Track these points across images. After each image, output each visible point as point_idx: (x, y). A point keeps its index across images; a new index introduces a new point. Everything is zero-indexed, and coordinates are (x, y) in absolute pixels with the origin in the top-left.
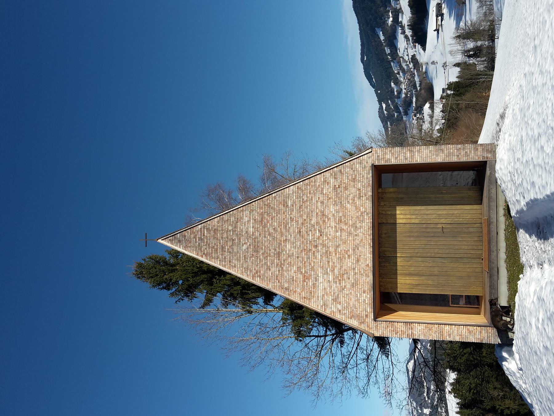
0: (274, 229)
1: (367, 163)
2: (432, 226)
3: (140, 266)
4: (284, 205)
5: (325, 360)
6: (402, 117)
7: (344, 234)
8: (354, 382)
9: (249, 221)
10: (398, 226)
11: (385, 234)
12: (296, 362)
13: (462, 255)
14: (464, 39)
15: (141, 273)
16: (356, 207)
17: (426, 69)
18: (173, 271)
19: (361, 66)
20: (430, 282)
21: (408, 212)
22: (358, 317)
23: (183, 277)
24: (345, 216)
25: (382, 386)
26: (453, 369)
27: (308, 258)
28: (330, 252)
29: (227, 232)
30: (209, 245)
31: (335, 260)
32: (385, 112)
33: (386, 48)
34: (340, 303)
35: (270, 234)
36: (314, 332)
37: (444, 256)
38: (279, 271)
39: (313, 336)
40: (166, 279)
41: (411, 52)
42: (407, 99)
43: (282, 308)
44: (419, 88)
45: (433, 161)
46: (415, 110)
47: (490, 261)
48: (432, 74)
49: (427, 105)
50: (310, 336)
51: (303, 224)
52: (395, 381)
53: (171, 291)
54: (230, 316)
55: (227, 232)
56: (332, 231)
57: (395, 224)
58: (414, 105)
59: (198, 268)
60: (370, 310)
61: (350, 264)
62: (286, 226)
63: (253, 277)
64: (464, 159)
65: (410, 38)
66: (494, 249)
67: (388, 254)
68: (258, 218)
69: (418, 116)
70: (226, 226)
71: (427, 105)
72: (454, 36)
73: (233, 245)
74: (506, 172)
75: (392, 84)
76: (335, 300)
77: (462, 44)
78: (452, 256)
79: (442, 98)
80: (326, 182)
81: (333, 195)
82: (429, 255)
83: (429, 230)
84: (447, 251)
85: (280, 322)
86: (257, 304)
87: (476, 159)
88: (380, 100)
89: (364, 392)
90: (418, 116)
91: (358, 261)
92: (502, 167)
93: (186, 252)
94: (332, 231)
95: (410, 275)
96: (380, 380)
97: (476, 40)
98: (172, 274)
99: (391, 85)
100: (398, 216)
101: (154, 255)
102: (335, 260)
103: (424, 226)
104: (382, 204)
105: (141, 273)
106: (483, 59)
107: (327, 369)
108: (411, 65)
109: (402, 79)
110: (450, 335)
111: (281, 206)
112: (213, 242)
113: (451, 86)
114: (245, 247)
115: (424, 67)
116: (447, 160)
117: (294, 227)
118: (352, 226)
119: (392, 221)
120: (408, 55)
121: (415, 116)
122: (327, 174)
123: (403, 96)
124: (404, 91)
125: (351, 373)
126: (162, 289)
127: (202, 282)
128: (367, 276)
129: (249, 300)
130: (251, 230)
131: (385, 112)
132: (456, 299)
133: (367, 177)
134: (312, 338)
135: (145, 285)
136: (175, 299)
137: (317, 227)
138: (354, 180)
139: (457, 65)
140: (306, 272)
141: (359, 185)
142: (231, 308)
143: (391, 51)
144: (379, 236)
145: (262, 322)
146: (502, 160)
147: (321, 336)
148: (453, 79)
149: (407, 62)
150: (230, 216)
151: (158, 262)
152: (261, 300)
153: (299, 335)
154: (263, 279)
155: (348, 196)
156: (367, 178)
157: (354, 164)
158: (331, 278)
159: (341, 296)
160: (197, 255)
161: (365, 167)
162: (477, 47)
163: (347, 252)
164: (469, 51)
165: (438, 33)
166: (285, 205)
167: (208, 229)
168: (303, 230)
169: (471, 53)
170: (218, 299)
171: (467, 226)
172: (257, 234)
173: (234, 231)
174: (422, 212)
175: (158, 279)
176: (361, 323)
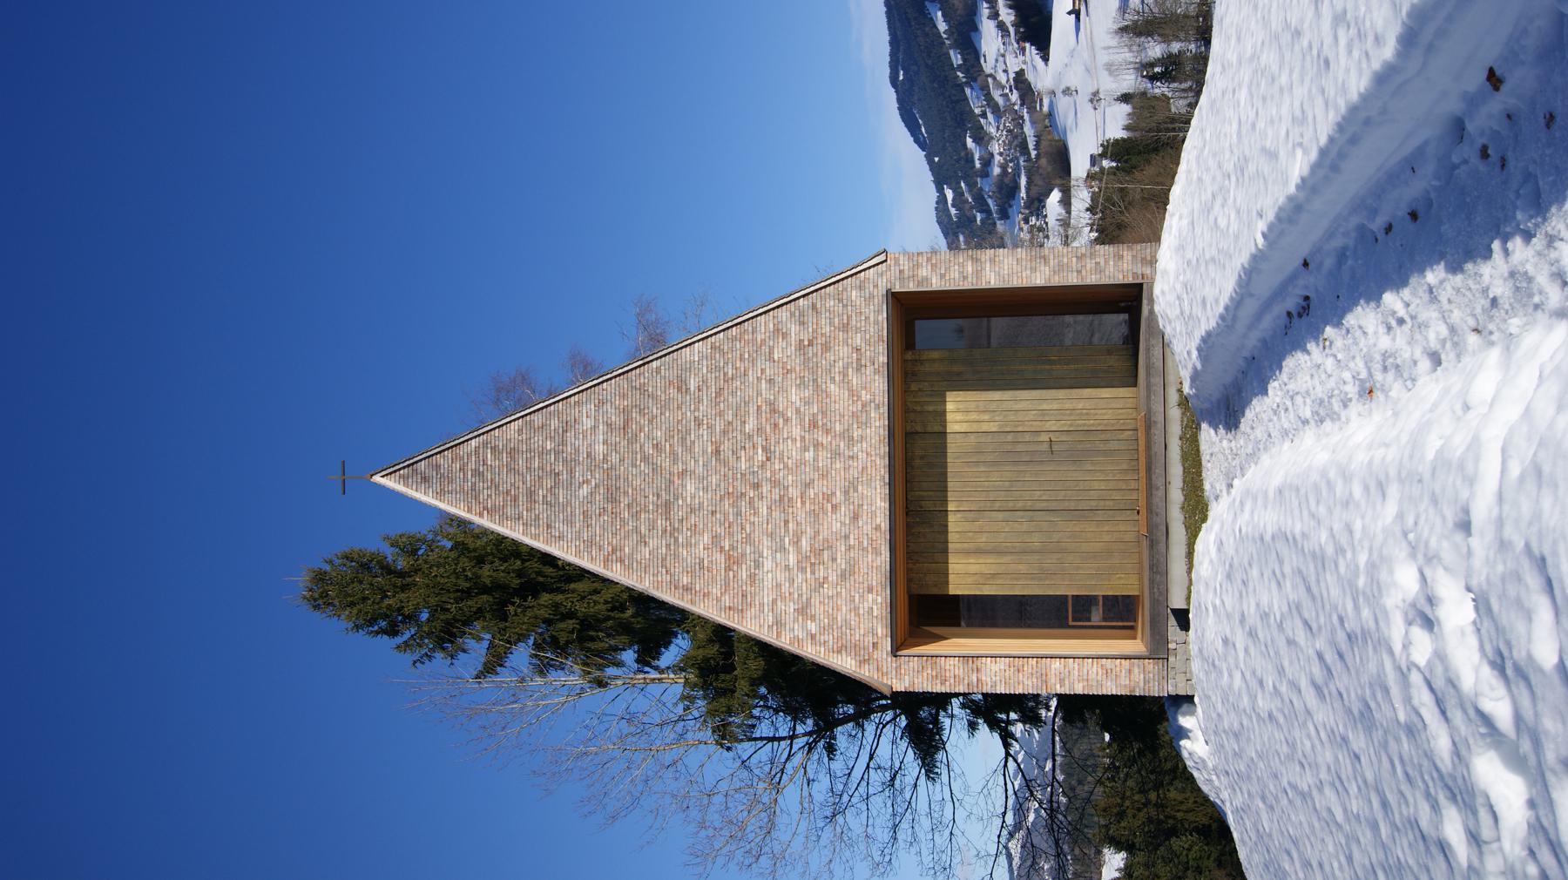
0: (656, 446)
1: (876, 286)
2: (1027, 438)
3: (320, 577)
4: (679, 389)
5: (791, 795)
6: (994, 224)
7: (822, 454)
8: (862, 846)
9: (595, 428)
10: (950, 439)
11: (922, 458)
12: (718, 799)
13: (1093, 504)
14: (1139, 34)
15: (324, 595)
16: (850, 390)
17: (1051, 105)
18: (404, 588)
19: (890, 95)
20: (1022, 568)
21: (972, 406)
22: (855, 649)
23: (433, 601)
24: (824, 413)
25: (925, 848)
26: (1118, 845)
27: (739, 514)
28: (790, 500)
29: (541, 454)
30: (497, 487)
31: (801, 516)
32: (953, 211)
33: (952, 52)
34: (813, 618)
35: (645, 459)
36: (764, 729)
37: (1053, 506)
38: (668, 546)
39: (761, 739)
40: (389, 607)
41: (1014, 64)
42: (1007, 180)
43: (682, 670)
44: (1033, 153)
45: (1025, 283)
46: (1026, 207)
47: (1150, 510)
48: (1066, 117)
49: (1055, 196)
50: (756, 739)
51: (724, 432)
52: (960, 840)
53: (399, 640)
54: (553, 701)
55: (541, 454)
56: (793, 450)
57: (943, 434)
58: (1023, 194)
59: (467, 579)
60: (882, 630)
61: (836, 526)
62: (684, 439)
63: (606, 561)
64: (1092, 279)
65: (1012, 30)
66: (1160, 482)
67: (928, 505)
68: (617, 420)
69: (1033, 220)
70: (538, 440)
71: (1055, 196)
72: (1116, 27)
73: (556, 485)
74: (1171, 298)
75: (969, 141)
76: (803, 611)
77: (1135, 48)
78: (1072, 505)
79: (1090, 177)
80: (780, 335)
81: (796, 363)
82: (1020, 505)
83: (1019, 448)
84: (1061, 495)
85: (676, 704)
86: (619, 664)
87: (1120, 279)
88: (941, 178)
89: (884, 863)
90: (1033, 220)
91: (856, 517)
92: (1166, 288)
93: (443, 506)
94: (793, 450)
95: (978, 552)
96: (921, 835)
97: (1166, 39)
98: (402, 596)
99: (965, 144)
100: (949, 417)
101: (357, 549)
102: (801, 516)
103: (1010, 438)
104: (914, 387)
105: (324, 595)
106: (1184, 86)
107: (796, 816)
108: (1015, 97)
109: (992, 130)
110: (1062, 681)
111: (673, 392)
112: (506, 480)
113: (1114, 149)
114: (585, 490)
115: (1046, 102)
116: (1056, 281)
117: (703, 441)
118: (842, 436)
119: (937, 428)
120: (1005, 71)
121: (1026, 221)
122: (783, 314)
123: (997, 171)
124: (998, 158)
125: (853, 821)
126: (377, 633)
127: (479, 614)
128: (877, 552)
129: (598, 653)
130: (600, 449)
131: (953, 211)
132: (1083, 605)
133: (875, 322)
134: (760, 744)
135: (335, 629)
136: (409, 657)
137: (759, 441)
138: (845, 327)
139: (1125, 98)
140: (732, 547)
141: (858, 340)
142: (557, 678)
143: (964, 60)
144: (908, 463)
145: (632, 709)
146: (1165, 272)
147: (780, 739)
148: (1116, 132)
149: (1003, 88)
150: (548, 419)
151: (365, 566)
152: (629, 656)
153: (725, 736)
154: (630, 567)
155: (833, 365)
156: (876, 322)
157: (845, 289)
158: (792, 559)
159: (815, 601)
160: (470, 511)
161: (872, 297)
162: (1170, 56)
163: (828, 497)
164: (1152, 65)
165: (1078, 18)
166: (682, 387)
167: (494, 449)
168: (726, 446)
169: (1157, 70)
170: (521, 655)
171: (1103, 437)
172: (615, 458)
173: (557, 453)
174: (1005, 406)
175: (368, 607)
176: (862, 662)
